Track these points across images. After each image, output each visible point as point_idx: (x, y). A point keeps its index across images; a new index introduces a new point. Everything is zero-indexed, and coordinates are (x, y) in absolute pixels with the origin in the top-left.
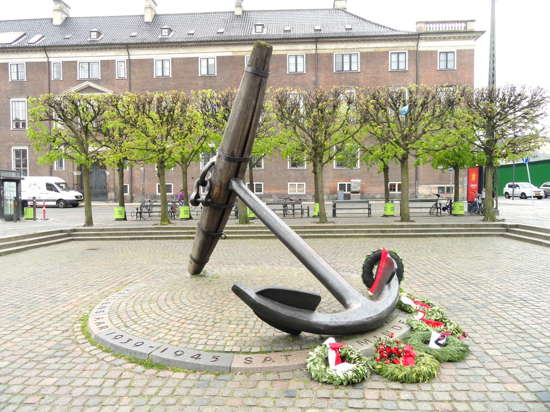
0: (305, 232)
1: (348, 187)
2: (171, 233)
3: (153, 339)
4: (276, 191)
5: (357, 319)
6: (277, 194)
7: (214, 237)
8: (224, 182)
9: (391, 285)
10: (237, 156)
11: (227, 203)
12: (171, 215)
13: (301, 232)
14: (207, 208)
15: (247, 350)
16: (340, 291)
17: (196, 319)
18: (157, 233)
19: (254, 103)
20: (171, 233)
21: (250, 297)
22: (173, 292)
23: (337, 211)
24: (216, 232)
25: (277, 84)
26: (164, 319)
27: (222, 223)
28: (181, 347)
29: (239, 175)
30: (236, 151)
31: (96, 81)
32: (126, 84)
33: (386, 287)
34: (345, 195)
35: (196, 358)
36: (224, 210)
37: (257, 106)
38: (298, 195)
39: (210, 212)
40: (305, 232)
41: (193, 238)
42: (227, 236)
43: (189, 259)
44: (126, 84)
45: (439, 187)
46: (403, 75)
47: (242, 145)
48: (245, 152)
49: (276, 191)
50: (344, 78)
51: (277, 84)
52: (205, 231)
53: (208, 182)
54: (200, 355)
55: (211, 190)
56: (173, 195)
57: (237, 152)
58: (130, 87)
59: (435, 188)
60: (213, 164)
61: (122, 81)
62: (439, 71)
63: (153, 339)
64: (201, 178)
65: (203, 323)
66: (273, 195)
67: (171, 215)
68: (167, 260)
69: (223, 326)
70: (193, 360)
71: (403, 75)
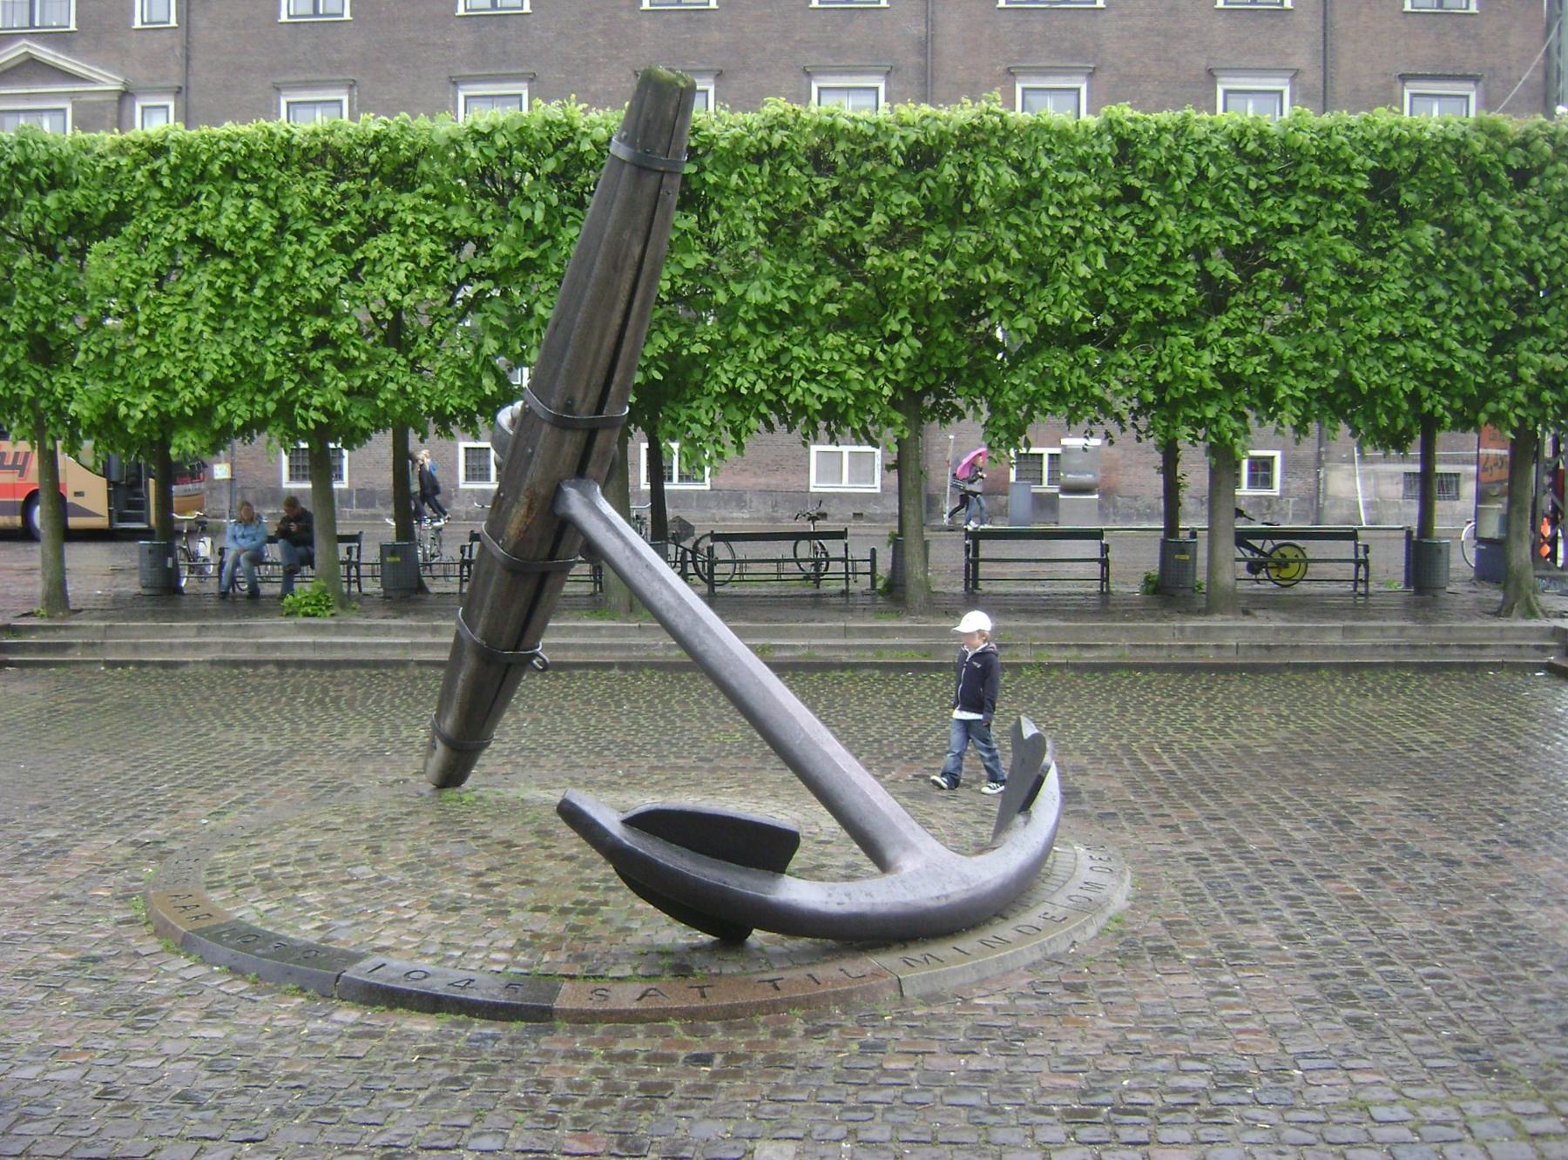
1: (1050, 464)
4: (762, 480)
5: (902, 899)
6: (766, 492)
7: (509, 665)
8: (542, 491)
9: (1034, 815)
10: (583, 413)
12: (349, 576)
16: (868, 828)
19: (637, 251)
23: (984, 569)
27: (537, 619)
31: (59, 39)
32: (172, 48)
33: (1020, 819)
34: (1037, 496)
36: (543, 577)
38: (849, 495)
44: (172, 48)
45: (1407, 474)
46: (1273, 26)
47: (599, 377)
49: (762, 480)
50: (1038, 27)
52: (480, 645)
56: (349, 492)
57: (583, 400)
58: (188, 58)
59: (1392, 476)
61: (157, 35)
62: (1410, 18)
66: (748, 497)
67: (349, 576)
71: (1273, 26)
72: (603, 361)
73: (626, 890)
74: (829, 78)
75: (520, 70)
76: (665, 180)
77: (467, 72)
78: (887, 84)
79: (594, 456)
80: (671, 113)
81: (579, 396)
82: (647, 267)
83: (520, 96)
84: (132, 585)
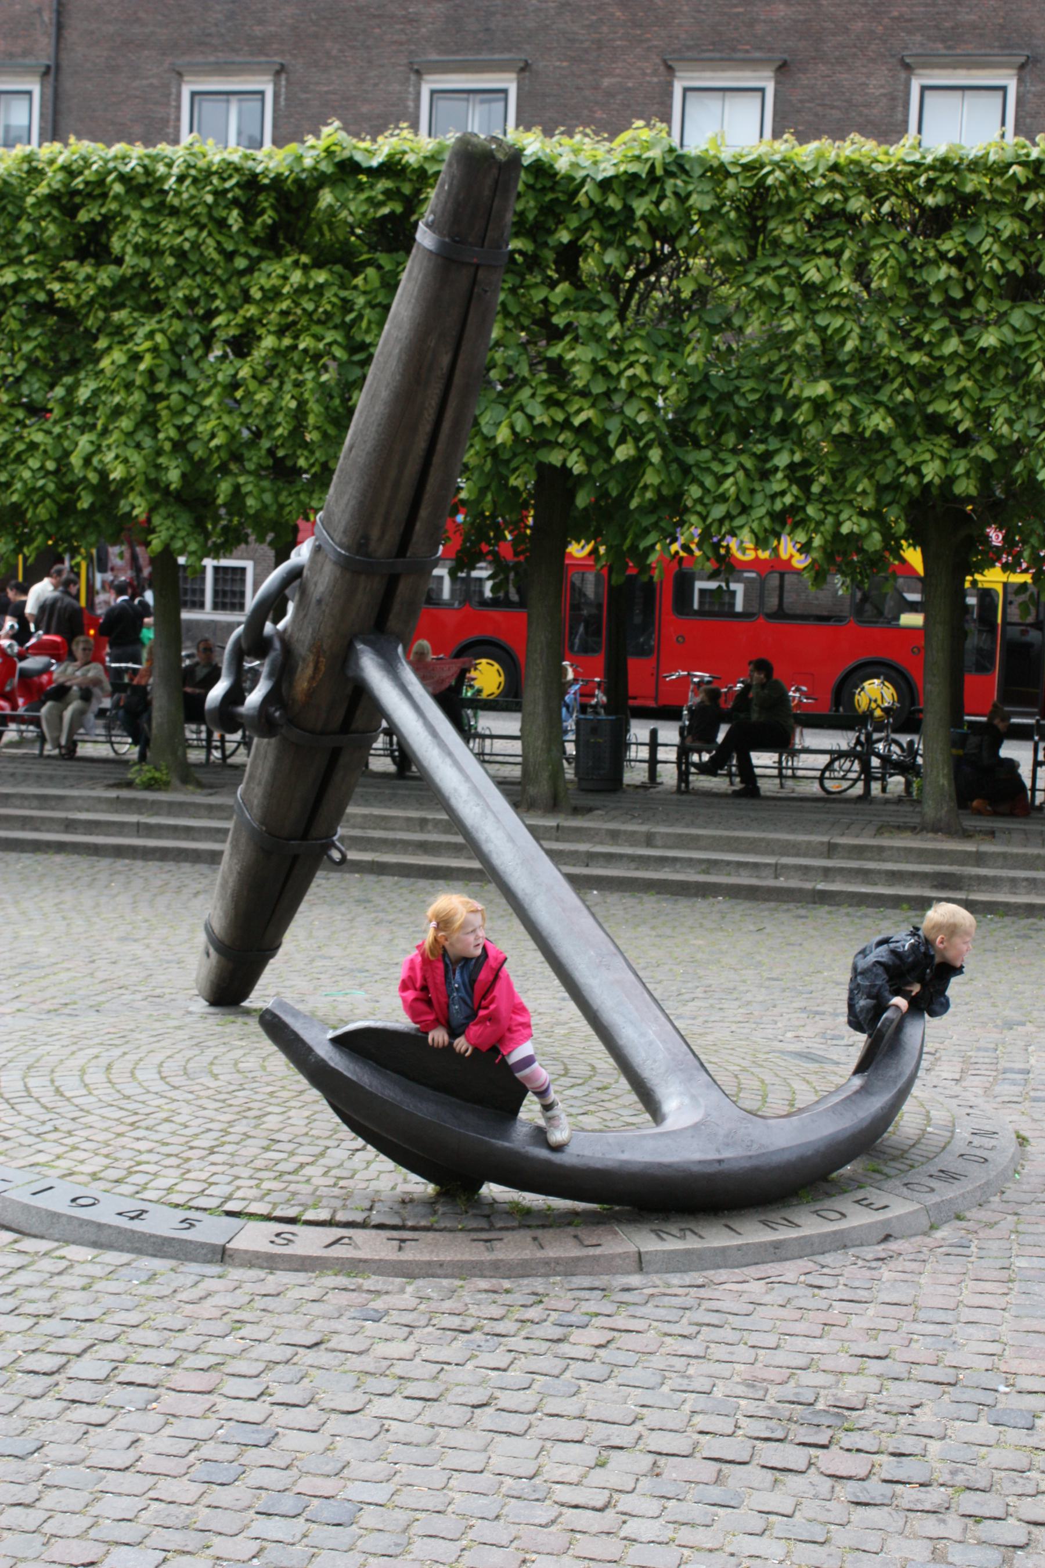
0: (591, 858)
2: (188, 832)
3: (15, 1164)
7: (295, 858)
10: (382, 547)
11: (346, 727)
13: (573, 857)
14: (268, 744)
15: (291, 1213)
17: (166, 1127)
18: (120, 828)
19: (445, 360)
20: (188, 832)
21: (310, 1050)
22: (117, 1052)
24: (305, 836)
25: (858, 26)
26: (62, 1121)
28: (95, 1189)
29: (393, 623)
30: (375, 533)
32: (39, 11)
35: (132, 1218)
36: (335, 754)
37: (458, 373)
39: (278, 760)
40: (591, 858)
41: (214, 858)
42: (352, 855)
43: (202, 938)
44: (39, 11)
47: (400, 511)
48: (415, 539)
51: (858, 26)
53: (277, 644)
54: (144, 1212)
55: (282, 675)
57: (381, 539)
58: (60, 27)
60: (296, 574)
63: (15, 1164)
64: (245, 629)
65: (183, 1140)
68: (137, 949)
69: (243, 1152)
70: (124, 1223)
72: (405, 493)
73: (330, 1110)
74: (937, 72)
75: (507, 56)
76: (481, 275)
77: (434, 57)
78: (1021, 81)
79: (396, 607)
80: (487, 192)
81: (375, 533)
82: (458, 380)
83: (505, 91)
84: (80, 745)
